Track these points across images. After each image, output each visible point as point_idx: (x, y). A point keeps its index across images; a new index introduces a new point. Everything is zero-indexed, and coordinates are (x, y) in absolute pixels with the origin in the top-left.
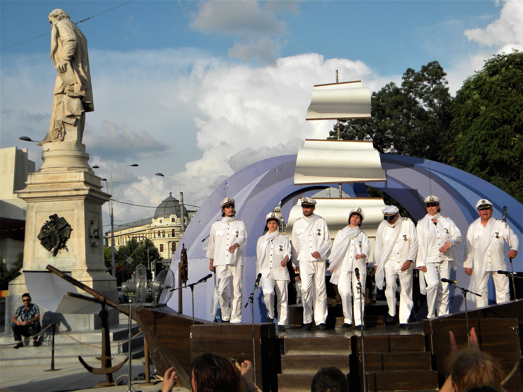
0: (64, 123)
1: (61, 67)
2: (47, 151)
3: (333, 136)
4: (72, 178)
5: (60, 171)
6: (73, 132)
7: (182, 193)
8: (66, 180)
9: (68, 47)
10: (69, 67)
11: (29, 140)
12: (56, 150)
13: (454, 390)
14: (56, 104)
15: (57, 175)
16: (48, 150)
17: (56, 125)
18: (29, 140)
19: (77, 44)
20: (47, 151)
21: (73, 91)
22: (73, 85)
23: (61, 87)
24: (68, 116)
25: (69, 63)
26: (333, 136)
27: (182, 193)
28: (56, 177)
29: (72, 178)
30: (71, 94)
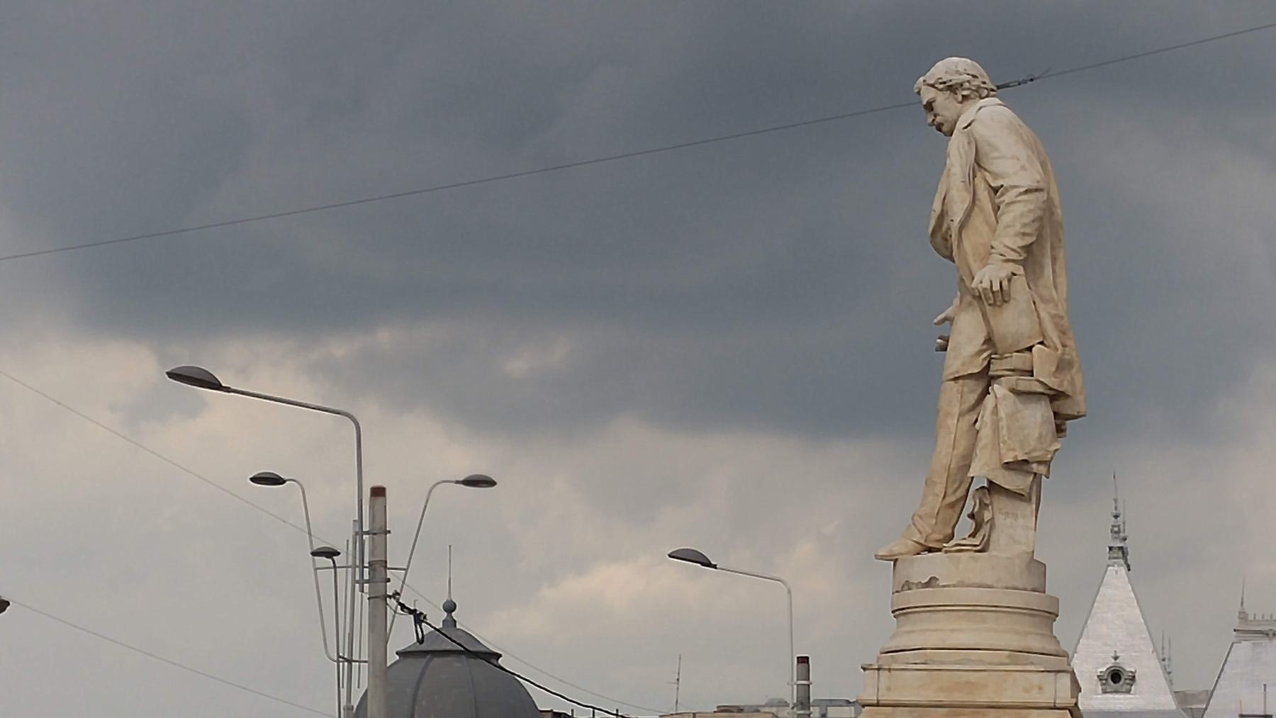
1: (996, 287)
2: (927, 585)
3: (500, 656)
5: (981, 662)
6: (1021, 521)
8: (1005, 699)
9: (1022, 215)
10: (1020, 283)
11: (277, 481)
12: (961, 584)
14: (956, 411)
15: (973, 677)
16: (931, 582)
17: (950, 491)
18: (277, 481)
19: (1049, 207)
20: (927, 585)
21: (1031, 373)
22: (1030, 349)
24: (1007, 466)
25: (1020, 270)
26: (500, 656)
28: (968, 683)
29: (1027, 690)
30: (1025, 384)
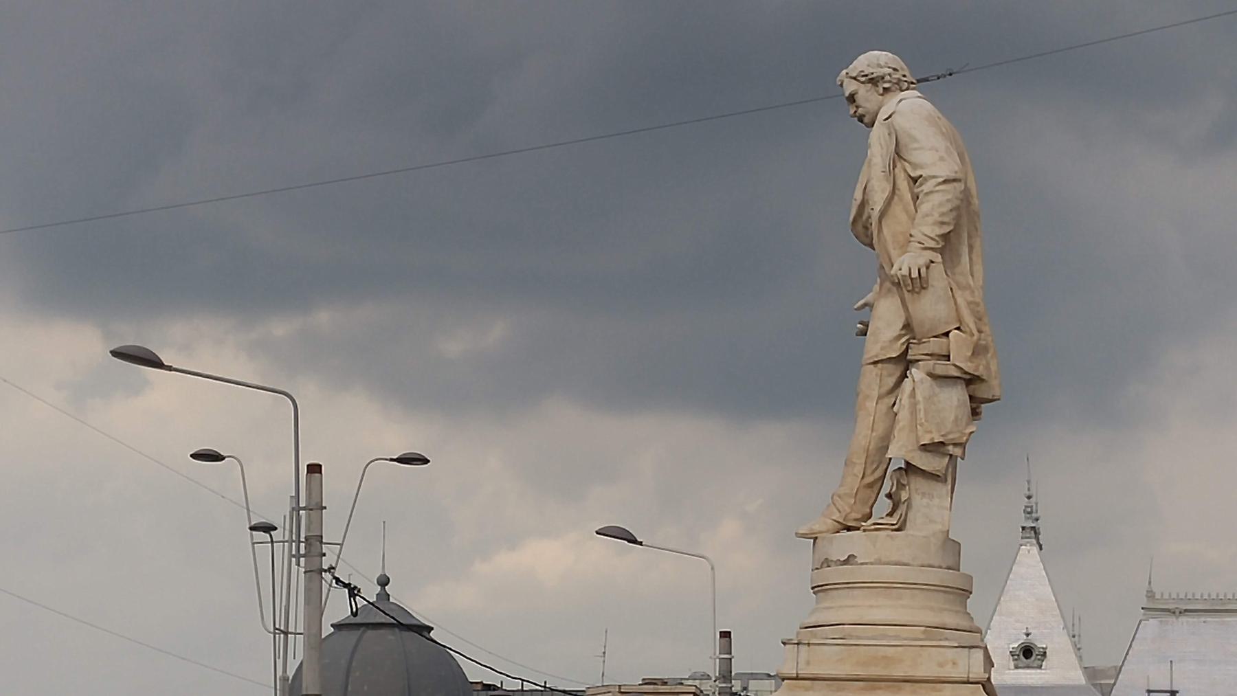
0: (909, 468)
1: (915, 274)
2: (846, 562)
4: (941, 665)
6: (936, 501)
7: (726, 635)
8: (920, 673)
10: (938, 271)
13: (1170, 193)
14: (875, 394)
17: (869, 471)
20: (846, 562)
21: (948, 358)
22: (947, 334)
23: (899, 337)
24: (924, 448)
25: (938, 258)
27: (726, 635)
28: (885, 657)
29: (941, 665)
30: (942, 368)
